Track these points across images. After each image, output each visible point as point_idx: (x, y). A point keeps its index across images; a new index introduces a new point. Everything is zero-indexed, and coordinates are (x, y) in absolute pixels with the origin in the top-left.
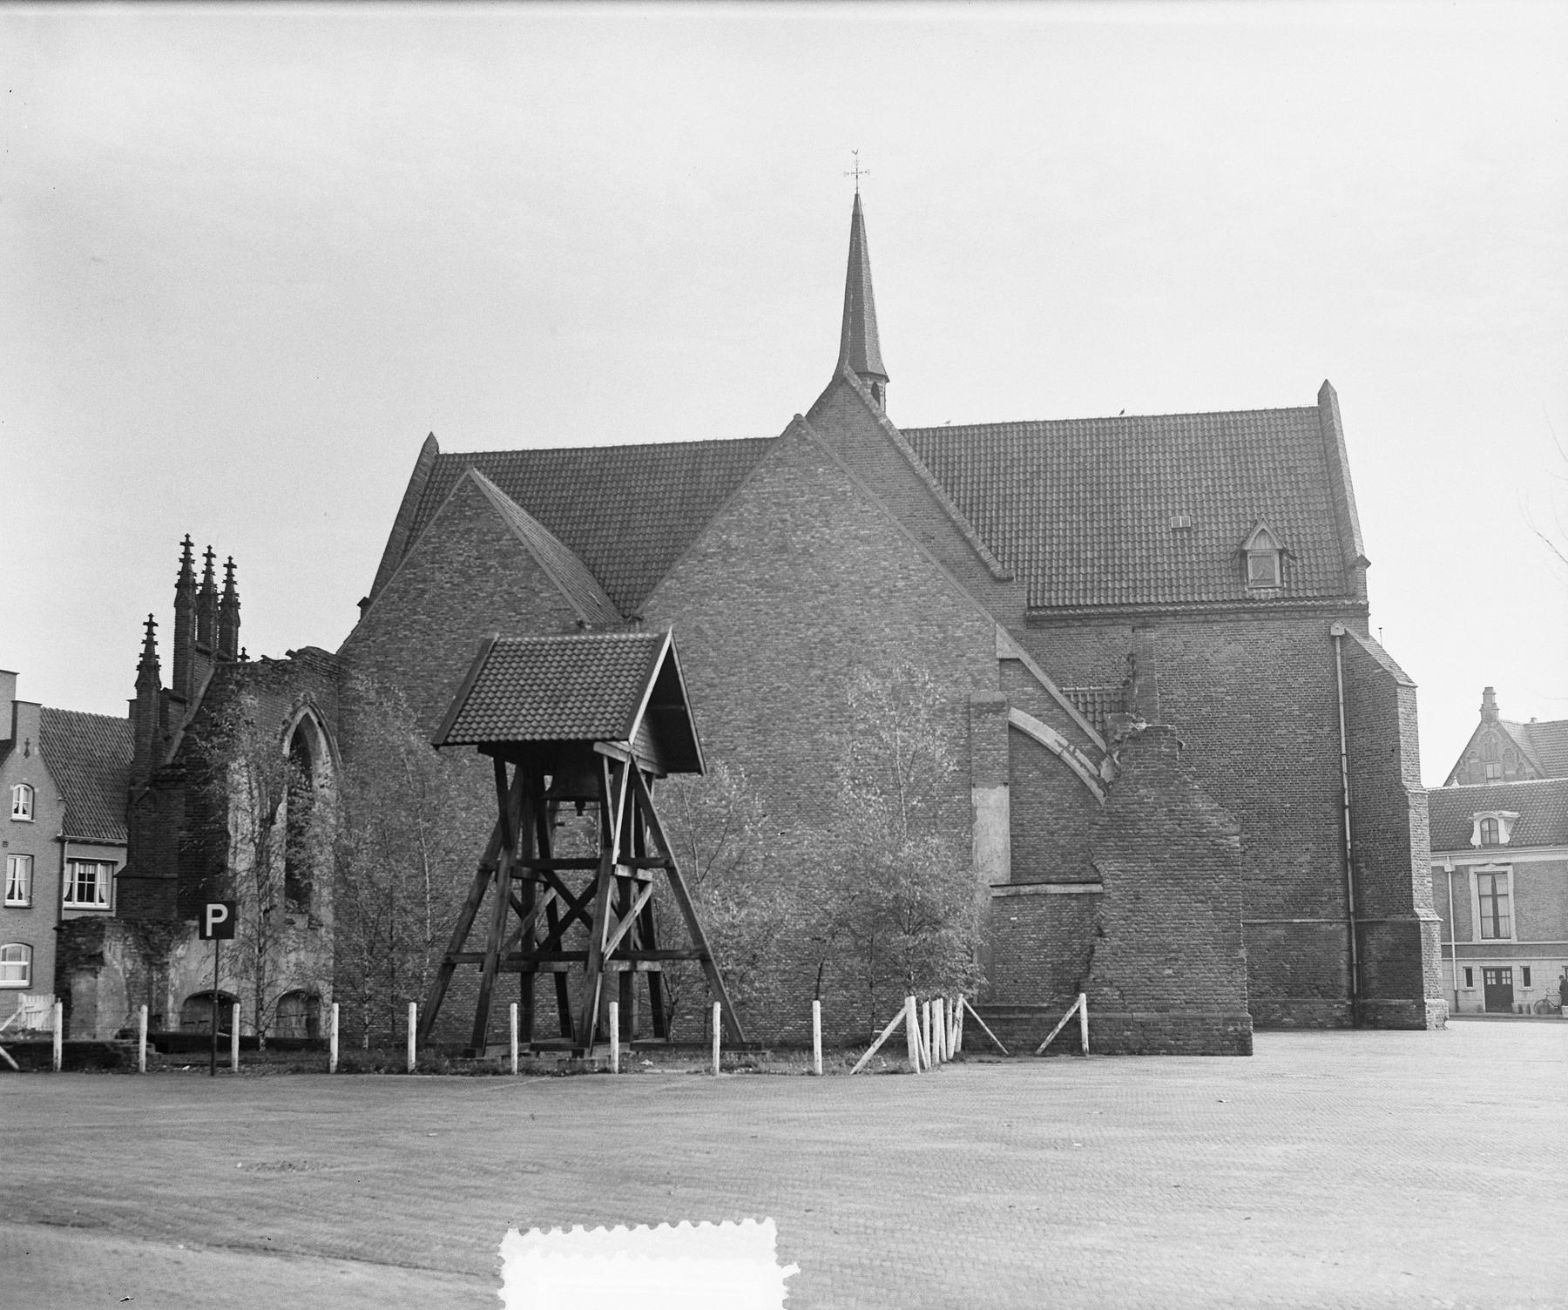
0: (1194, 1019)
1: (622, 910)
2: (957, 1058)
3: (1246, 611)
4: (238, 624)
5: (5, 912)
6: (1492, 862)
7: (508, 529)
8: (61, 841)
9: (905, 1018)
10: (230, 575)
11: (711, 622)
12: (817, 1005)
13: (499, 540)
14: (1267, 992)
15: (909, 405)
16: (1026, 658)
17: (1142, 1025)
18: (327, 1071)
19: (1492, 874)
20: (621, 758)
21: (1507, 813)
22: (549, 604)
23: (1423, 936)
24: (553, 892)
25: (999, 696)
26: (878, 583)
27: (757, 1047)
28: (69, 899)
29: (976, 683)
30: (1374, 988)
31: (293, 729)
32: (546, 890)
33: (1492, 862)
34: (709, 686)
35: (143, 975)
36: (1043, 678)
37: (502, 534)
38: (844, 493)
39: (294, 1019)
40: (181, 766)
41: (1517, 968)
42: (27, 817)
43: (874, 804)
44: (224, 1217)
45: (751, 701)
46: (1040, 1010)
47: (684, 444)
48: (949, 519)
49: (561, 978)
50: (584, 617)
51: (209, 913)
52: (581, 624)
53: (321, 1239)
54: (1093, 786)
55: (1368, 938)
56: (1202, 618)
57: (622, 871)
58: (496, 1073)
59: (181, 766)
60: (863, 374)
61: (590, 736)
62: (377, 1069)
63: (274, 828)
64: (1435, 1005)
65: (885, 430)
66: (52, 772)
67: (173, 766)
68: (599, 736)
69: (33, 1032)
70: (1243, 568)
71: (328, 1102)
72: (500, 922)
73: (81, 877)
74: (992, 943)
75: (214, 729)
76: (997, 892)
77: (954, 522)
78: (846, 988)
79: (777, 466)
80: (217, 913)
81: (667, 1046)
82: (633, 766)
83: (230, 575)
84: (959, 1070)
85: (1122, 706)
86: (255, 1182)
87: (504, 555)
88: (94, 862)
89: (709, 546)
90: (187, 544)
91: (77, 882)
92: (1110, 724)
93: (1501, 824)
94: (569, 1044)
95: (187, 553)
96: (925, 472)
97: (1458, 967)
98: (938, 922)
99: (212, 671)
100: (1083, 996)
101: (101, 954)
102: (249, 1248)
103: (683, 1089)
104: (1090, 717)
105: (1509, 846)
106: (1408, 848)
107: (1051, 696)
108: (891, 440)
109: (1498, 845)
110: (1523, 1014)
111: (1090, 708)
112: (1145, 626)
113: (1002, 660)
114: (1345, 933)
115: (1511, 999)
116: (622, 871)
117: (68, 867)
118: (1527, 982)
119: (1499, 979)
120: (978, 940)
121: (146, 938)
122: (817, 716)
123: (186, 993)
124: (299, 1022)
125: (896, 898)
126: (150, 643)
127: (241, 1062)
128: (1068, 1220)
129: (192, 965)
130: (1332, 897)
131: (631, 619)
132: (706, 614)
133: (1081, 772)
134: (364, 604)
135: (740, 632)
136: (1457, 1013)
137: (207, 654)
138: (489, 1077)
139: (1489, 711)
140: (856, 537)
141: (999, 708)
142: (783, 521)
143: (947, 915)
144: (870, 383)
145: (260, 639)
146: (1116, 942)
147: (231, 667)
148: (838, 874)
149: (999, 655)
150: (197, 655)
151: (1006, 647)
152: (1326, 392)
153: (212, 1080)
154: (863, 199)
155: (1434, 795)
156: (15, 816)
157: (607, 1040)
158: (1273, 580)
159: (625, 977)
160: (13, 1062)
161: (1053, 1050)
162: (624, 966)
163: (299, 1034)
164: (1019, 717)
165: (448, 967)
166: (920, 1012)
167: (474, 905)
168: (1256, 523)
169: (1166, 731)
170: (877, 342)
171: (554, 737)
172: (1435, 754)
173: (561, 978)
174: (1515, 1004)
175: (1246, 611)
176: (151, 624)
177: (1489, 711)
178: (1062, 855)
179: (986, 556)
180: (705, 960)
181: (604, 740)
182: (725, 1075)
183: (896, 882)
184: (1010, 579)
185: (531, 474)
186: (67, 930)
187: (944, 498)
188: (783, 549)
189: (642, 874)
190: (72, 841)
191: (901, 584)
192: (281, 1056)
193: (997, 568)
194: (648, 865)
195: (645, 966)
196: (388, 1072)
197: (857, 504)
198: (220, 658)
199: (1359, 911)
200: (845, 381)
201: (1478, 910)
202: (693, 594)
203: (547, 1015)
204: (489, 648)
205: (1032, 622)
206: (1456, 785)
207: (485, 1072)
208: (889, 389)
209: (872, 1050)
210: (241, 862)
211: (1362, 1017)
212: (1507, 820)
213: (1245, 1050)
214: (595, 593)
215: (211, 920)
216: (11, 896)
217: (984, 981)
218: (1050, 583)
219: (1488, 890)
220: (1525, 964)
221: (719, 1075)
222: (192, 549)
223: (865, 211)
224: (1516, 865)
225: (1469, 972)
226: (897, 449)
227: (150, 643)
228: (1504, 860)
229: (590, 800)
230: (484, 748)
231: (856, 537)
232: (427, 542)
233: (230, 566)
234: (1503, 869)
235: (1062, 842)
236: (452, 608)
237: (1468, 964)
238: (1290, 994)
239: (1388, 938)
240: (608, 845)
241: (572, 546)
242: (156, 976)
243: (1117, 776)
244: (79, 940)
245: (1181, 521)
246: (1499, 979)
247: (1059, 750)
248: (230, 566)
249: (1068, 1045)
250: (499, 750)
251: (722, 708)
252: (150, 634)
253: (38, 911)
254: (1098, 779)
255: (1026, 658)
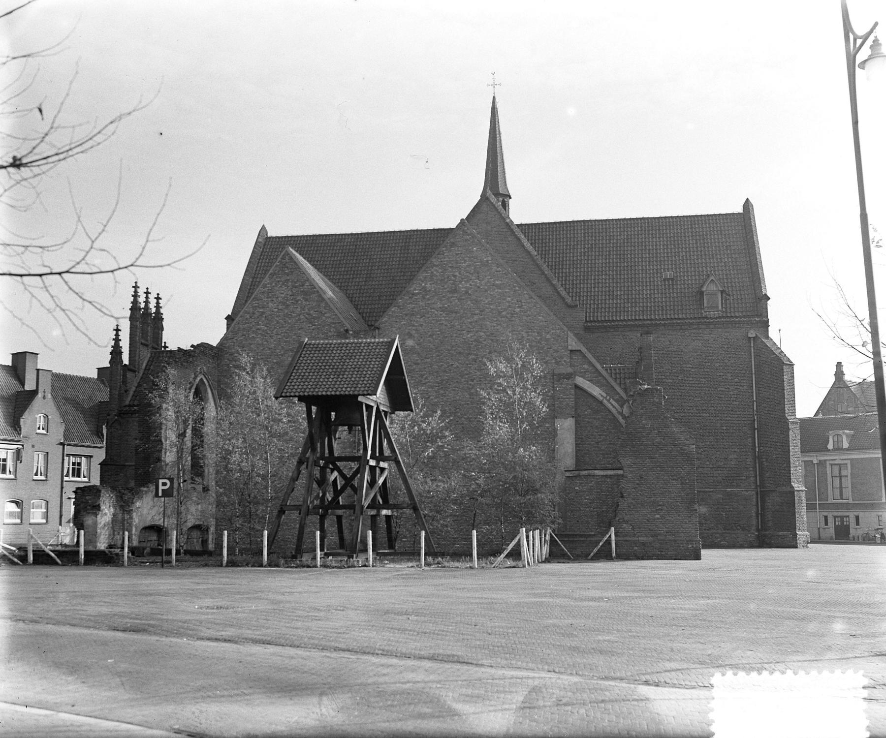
0: (670, 540)
1: (372, 483)
2: (547, 561)
3: (702, 323)
4: (163, 329)
5: (34, 483)
6: (838, 458)
7: (308, 280)
8: (62, 444)
9: (519, 540)
10: (158, 303)
11: (416, 330)
12: (474, 532)
13: (303, 286)
14: (713, 528)
15: (521, 212)
16: (584, 350)
17: (644, 544)
18: (221, 565)
19: (839, 465)
20: (372, 404)
21: (848, 432)
22: (330, 320)
23: (796, 498)
24: (336, 474)
25: (570, 370)
26: (505, 310)
27: (443, 555)
28: (67, 476)
29: (557, 363)
30: (770, 528)
31: (195, 386)
32: (332, 472)
33: (838, 458)
34: (416, 364)
35: (120, 516)
36: (593, 360)
37: (305, 281)
38: (487, 261)
39: (195, 540)
40: (134, 405)
41: (852, 515)
42: (44, 432)
43: (502, 430)
44: (200, 628)
45: (437, 372)
46: (590, 536)
47: (400, 232)
48: (543, 273)
49: (339, 518)
50: (349, 326)
51: (160, 484)
52: (347, 331)
53: (250, 636)
54: (620, 418)
55: (767, 499)
56: (678, 327)
57: (372, 463)
58: (308, 567)
59: (134, 405)
60: (497, 194)
61: (356, 393)
62: (247, 565)
63: (186, 439)
64: (802, 535)
65: (509, 225)
66: (59, 408)
67: (129, 406)
68: (361, 392)
69: (66, 545)
70: (701, 299)
71: (227, 580)
72: (309, 490)
73: (74, 464)
74: (565, 501)
75: (154, 386)
76: (568, 474)
77: (546, 275)
78: (488, 524)
79: (451, 246)
80: (164, 484)
81: (395, 554)
82: (378, 408)
83: (158, 303)
84: (548, 566)
85: (635, 375)
86: (204, 614)
87: (305, 293)
88: (80, 456)
89: (415, 289)
90: (136, 287)
91: (71, 467)
92: (628, 385)
93: (844, 437)
94: (346, 550)
95: (136, 292)
96: (530, 248)
97: (819, 515)
98: (537, 490)
99: (149, 355)
100: (613, 529)
101: (99, 506)
102: (217, 640)
103: (406, 574)
104: (618, 381)
105: (847, 449)
106: (789, 451)
107: (597, 370)
108: (512, 230)
109: (842, 449)
110: (855, 541)
111: (618, 376)
112: (647, 333)
113: (571, 351)
114: (755, 496)
115: (849, 533)
116: (372, 463)
117: (66, 458)
118: (858, 524)
119: (842, 521)
120: (557, 499)
121: (121, 497)
122: (472, 380)
123: (142, 526)
124: (198, 541)
125: (514, 477)
126: (117, 340)
127: (177, 561)
128: (599, 630)
129: (147, 509)
130: (748, 477)
131: (372, 327)
132: (414, 326)
133: (613, 410)
134: (228, 318)
135: (431, 336)
136: (817, 539)
137: (147, 345)
138: (305, 569)
139: (839, 373)
140: (494, 285)
141: (570, 376)
142: (455, 276)
143: (541, 486)
144: (501, 199)
145: (175, 337)
146: (630, 500)
147: (159, 353)
148: (485, 464)
149: (570, 348)
150: (141, 347)
151: (573, 343)
152: (747, 205)
153: (162, 570)
154: (497, 99)
155: (804, 422)
156: (38, 431)
157: (365, 550)
158: (717, 307)
159: (373, 517)
160: (58, 561)
161: (597, 558)
162: (373, 512)
163: (198, 547)
164: (580, 381)
165: (282, 512)
166: (527, 537)
167: (295, 479)
168: (708, 276)
169: (657, 390)
170: (503, 162)
171: (338, 393)
172: (807, 399)
173: (339, 518)
174: (851, 536)
175: (702, 323)
176: (117, 330)
177: (839, 373)
178: (603, 454)
179: (563, 293)
180: (415, 509)
181: (364, 395)
182: (427, 568)
183: (515, 469)
184: (576, 306)
185: (322, 248)
186: (80, 493)
187: (540, 262)
188: (455, 291)
189: (382, 464)
190: (68, 445)
191: (517, 310)
192: (195, 558)
193: (569, 300)
194: (385, 459)
195: (384, 512)
196: (253, 566)
197: (494, 268)
198: (153, 348)
199: (762, 485)
200: (487, 199)
201: (832, 484)
202: (406, 315)
203: (333, 537)
204: (302, 347)
205: (587, 329)
206: (821, 416)
207: (303, 566)
208: (511, 202)
209: (503, 556)
210: (169, 457)
211: (763, 542)
212: (847, 435)
213: (698, 557)
214: (353, 313)
215: (161, 488)
216: (36, 474)
217: (561, 521)
218: (598, 308)
219: (836, 473)
220: (856, 514)
221: (423, 567)
222: (139, 290)
223: (498, 105)
224: (852, 460)
225: (826, 518)
226: (516, 236)
227: (117, 340)
228: (844, 457)
229: (356, 425)
230: (301, 399)
231: (494, 285)
232: (265, 286)
233: (158, 298)
234: (845, 462)
235: (603, 448)
236: (278, 322)
237: (825, 514)
238: (725, 529)
239: (778, 499)
240: (365, 449)
241: (340, 287)
242: (127, 517)
243: (631, 414)
244: (87, 498)
245: (668, 275)
246: (842, 521)
247: (601, 398)
248: (158, 298)
249: (605, 555)
250: (308, 400)
251: (422, 376)
252: (117, 335)
253: (50, 482)
254: (621, 414)
255: (584, 350)
